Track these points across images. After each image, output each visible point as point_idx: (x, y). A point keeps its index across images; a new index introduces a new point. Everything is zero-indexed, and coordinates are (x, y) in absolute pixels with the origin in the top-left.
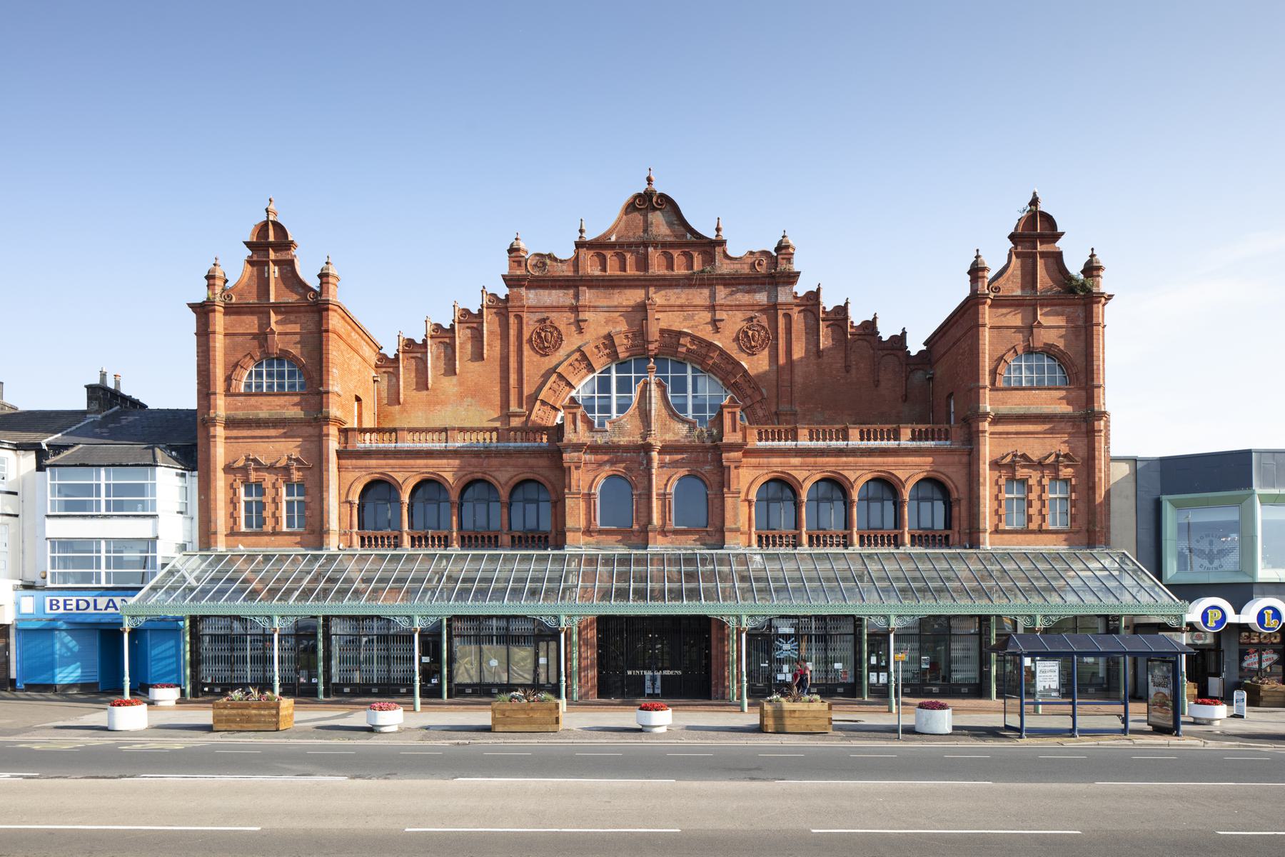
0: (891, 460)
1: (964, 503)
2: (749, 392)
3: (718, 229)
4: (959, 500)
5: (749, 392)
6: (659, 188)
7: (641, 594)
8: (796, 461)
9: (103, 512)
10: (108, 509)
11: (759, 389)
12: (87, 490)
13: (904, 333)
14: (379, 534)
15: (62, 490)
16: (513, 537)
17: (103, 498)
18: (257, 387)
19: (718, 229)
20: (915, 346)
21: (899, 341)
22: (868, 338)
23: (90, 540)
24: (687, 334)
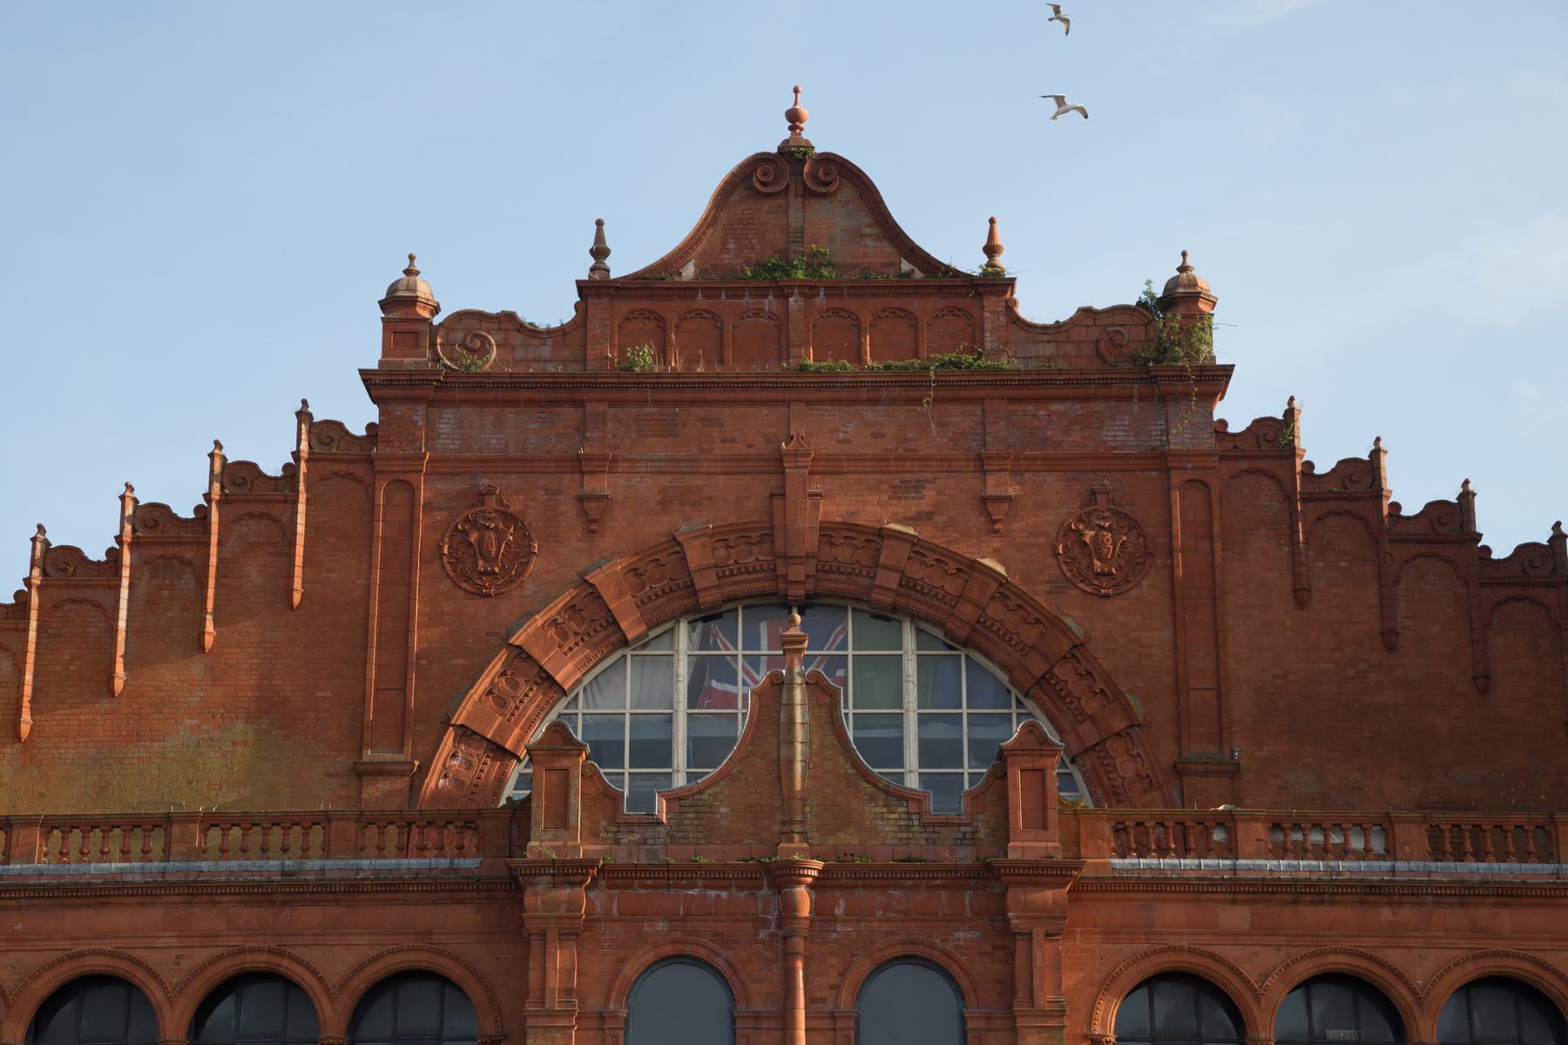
2: (1092, 706)
3: (991, 249)
5: (1092, 706)
6: (821, 138)
13: (1467, 496)
19: (991, 249)
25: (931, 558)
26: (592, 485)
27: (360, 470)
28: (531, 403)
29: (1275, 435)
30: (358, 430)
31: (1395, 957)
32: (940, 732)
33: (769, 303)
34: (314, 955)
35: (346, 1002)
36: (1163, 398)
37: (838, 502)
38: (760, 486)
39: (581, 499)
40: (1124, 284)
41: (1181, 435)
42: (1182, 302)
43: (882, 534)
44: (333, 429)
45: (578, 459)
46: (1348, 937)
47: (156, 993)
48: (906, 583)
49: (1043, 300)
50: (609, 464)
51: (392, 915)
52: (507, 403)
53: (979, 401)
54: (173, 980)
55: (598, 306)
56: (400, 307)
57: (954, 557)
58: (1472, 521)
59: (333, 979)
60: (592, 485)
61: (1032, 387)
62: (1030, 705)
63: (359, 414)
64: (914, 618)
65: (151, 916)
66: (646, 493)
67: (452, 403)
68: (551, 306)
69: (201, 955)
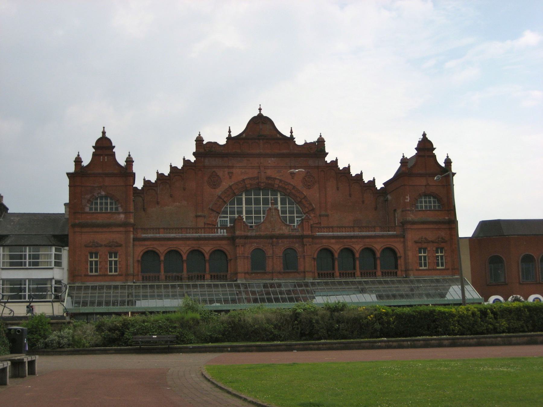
0: (372, 240)
2: (307, 206)
3: (291, 132)
4: (400, 257)
5: (307, 206)
6: (265, 113)
8: (333, 241)
9: (27, 267)
10: (29, 265)
12: (21, 257)
14: (323, 272)
15: (11, 257)
16: (211, 276)
17: (27, 260)
18: (95, 209)
19: (291, 132)
20: (379, 185)
23: (21, 280)
29: (335, 163)
30: (193, 161)
31: (354, 246)
34: (204, 248)
35: (209, 254)
37: (269, 172)
40: (313, 139)
42: (321, 142)
43: (275, 179)
44: (189, 161)
46: (173, 245)
47: (182, 253)
49: (299, 141)
50: (232, 167)
51: (215, 242)
54: (185, 251)
56: (199, 140)
59: (207, 251)
62: (298, 205)
63: (193, 159)
64: (280, 192)
65: (181, 242)
66: (241, 172)
68: (222, 141)
69: (188, 248)
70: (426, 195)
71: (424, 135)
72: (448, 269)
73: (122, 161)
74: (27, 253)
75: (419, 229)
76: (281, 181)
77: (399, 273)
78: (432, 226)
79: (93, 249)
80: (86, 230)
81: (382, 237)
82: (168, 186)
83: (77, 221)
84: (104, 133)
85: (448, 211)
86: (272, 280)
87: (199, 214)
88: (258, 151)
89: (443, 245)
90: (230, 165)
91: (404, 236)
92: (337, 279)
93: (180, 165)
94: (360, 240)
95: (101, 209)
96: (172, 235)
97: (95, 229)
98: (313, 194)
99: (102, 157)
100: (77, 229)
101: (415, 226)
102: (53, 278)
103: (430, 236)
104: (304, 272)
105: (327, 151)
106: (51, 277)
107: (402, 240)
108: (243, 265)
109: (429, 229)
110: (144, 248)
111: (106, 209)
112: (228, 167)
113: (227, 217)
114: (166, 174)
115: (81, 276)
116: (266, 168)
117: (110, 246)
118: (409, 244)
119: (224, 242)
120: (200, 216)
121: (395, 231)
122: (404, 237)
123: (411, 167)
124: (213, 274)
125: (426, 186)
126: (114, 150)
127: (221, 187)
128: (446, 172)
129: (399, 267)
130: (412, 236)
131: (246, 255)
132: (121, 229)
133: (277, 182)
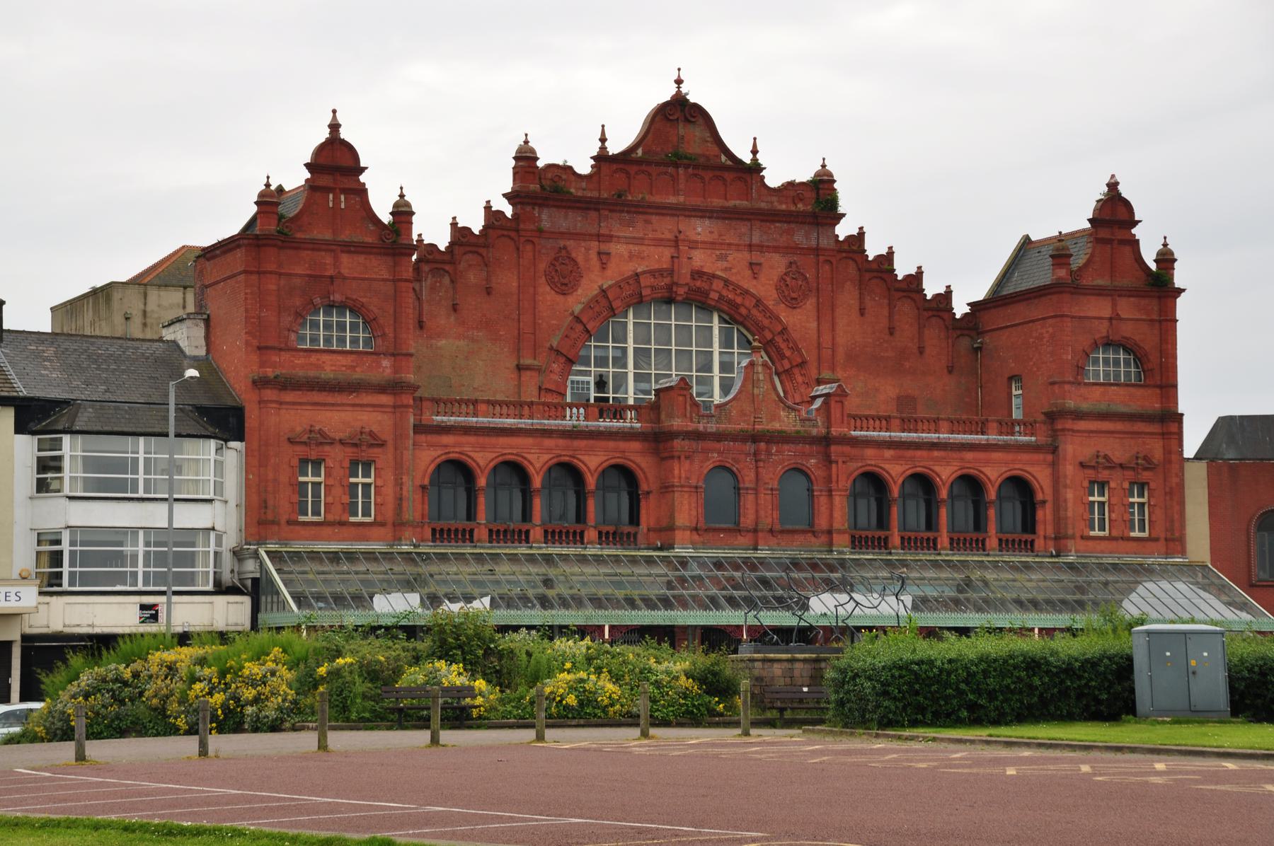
1: (1049, 506)
3: (755, 152)
4: (1044, 502)
7: (545, 603)
8: (888, 453)
9: (141, 494)
11: (799, 350)
12: (121, 465)
13: (891, 253)
19: (755, 152)
20: (960, 308)
21: (945, 298)
22: (913, 295)
24: (719, 278)
25: (731, 288)
26: (604, 247)
27: (513, 234)
28: (579, 208)
29: (858, 239)
31: (937, 468)
32: (726, 358)
33: (671, 170)
36: (818, 224)
37: (700, 259)
38: (667, 253)
39: (599, 253)
41: (824, 243)
43: (714, 276)
45: (598, 235)
46: (922, 462)
47: (531, 470)
48: (721, 297)
49: (773, 178)
50: (609, 238)
51: (611, 444)
52: (569, 207)
53: (749, 220)
54: (538, 466)
55: (605, 168)
57: (739, 287)
58: (892, 264)
60: (604, 247)
61: (769, 217)
64: (719, 310)
66: (631, 252)
67: (547, 206)
69: (547, 457)
70: (1108, 344)
71: (1113, 186)
72: (1156, 540)
73: (383, 210)
74: (141, 456)
75: (1092, 432)
76: (727, 282)
77: (1039, 543)
78: (1119, 426)
79: (311, 449)
80: (289, 396)
81: (1005, 447)
82: (446, 280)
83: (270, 373)
84: (335, 127)
85: (1161, 387)
86: (756, 549)
87: (528, 361)
88: (672, 200)
89: (1146, 476)
90: (604, 231)
91: (1057, 447)
92: (947, 555)
93: (476, 223)
94: (951, 454)
95: (328, 340)
96: (510, 422)
97: (317, 397)
98: (800, 321)
99: (331, 196)
100: (269, 394)
101: (1083, 425)
102: (213, 529)
103: (1119, 450)
104: (830, 532)
105: (841, 210)
106: (209, 525)
107: (1050, 457)
108: (685, 511)
109: (1112, 432)
110: (440, 452)
111: (342, 340)
112: (599, 237)
113: (588, 373)
114: (442, 248)
115: (278, 524)
116: (693, 245)
117: (355, 445)
118: (1069, 470)
119: (636, 445)
120: (528, 368)
121: (1032, 435)
122: (1054, 450)
123: (1080, 269)
124: (605, 529)
125: (1111, 319)
126: (362, 178)
127: (580, 291)
128: (1159, 286)
129: (1040, 529)
130: (1074, 449)
131: (693, 482)
132: (385, 399)
133: (718, 285)
